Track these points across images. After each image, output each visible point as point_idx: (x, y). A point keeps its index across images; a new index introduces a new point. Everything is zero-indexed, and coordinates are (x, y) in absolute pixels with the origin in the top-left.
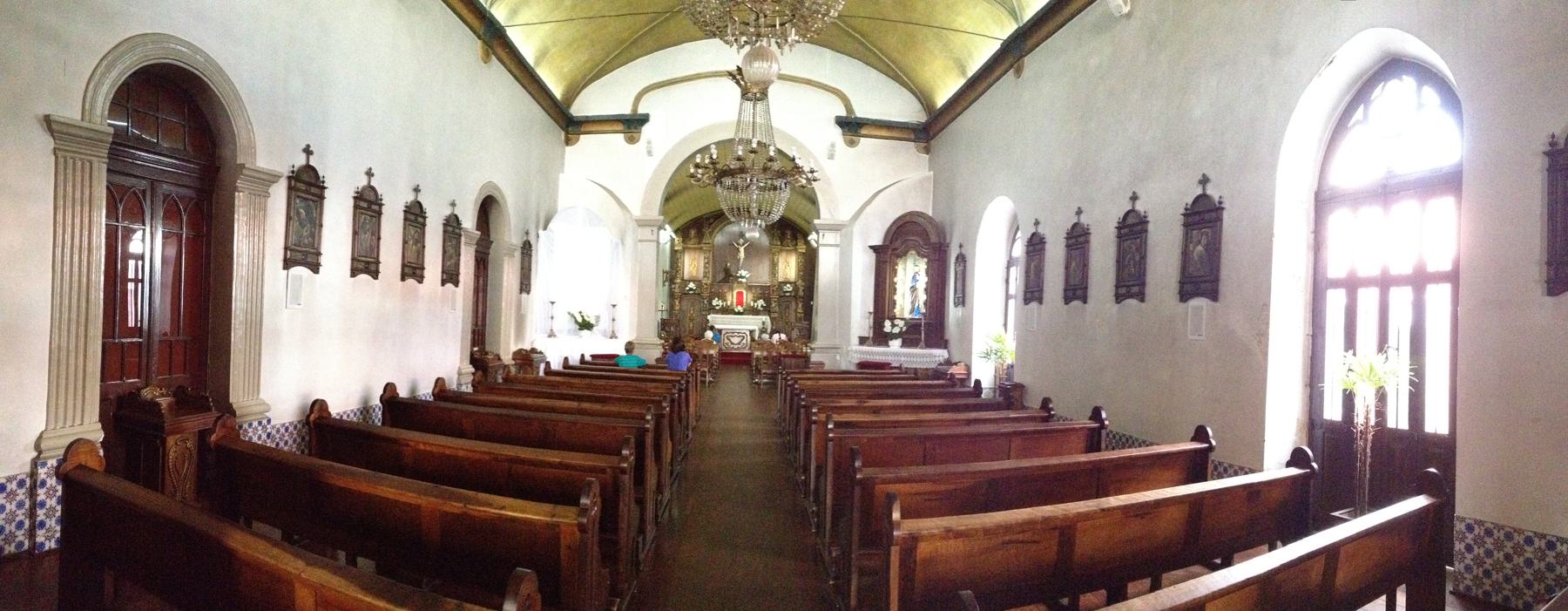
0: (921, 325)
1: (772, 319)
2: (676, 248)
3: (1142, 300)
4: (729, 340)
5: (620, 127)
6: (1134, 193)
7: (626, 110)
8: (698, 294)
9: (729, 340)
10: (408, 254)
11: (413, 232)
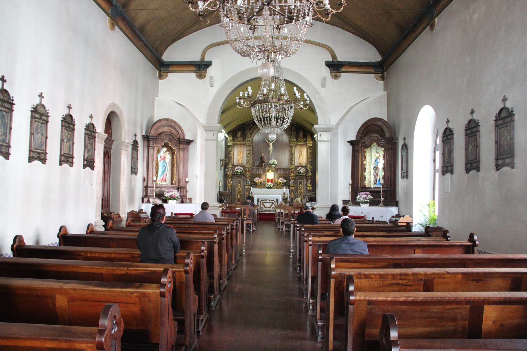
0: (380, 192)
1: (291, 191)
2: (229, 144)
3: (513, 167)
4: (263, 205)
5: (194, 69)
6: (504, 96)
7: (196, 57)
8: (242, 174)
9: (263, 205)
10: (64, 148)
11: (67, 134)
